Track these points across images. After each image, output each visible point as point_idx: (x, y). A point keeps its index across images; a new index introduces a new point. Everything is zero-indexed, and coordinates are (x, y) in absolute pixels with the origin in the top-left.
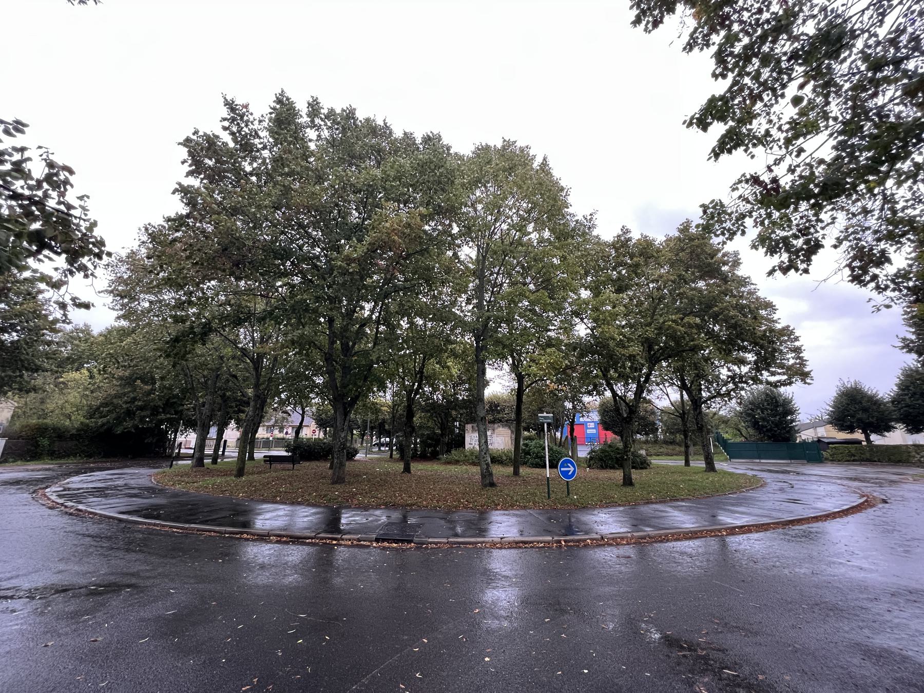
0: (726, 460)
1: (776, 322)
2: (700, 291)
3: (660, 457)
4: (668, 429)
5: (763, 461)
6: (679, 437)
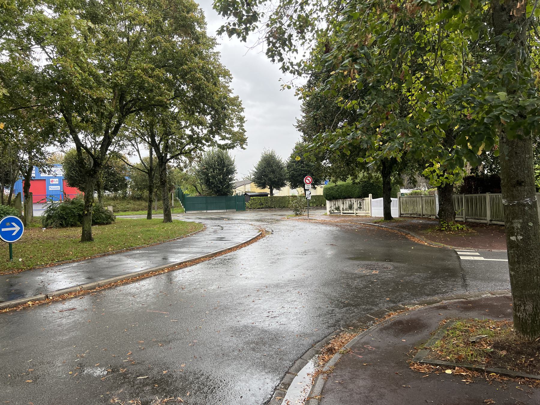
0: (182, 212)
1: (230, 91)
2: (173, 45)
3: (127, 213)
4: (136, 185)
5: (208, 211)
6: (146, 193)
